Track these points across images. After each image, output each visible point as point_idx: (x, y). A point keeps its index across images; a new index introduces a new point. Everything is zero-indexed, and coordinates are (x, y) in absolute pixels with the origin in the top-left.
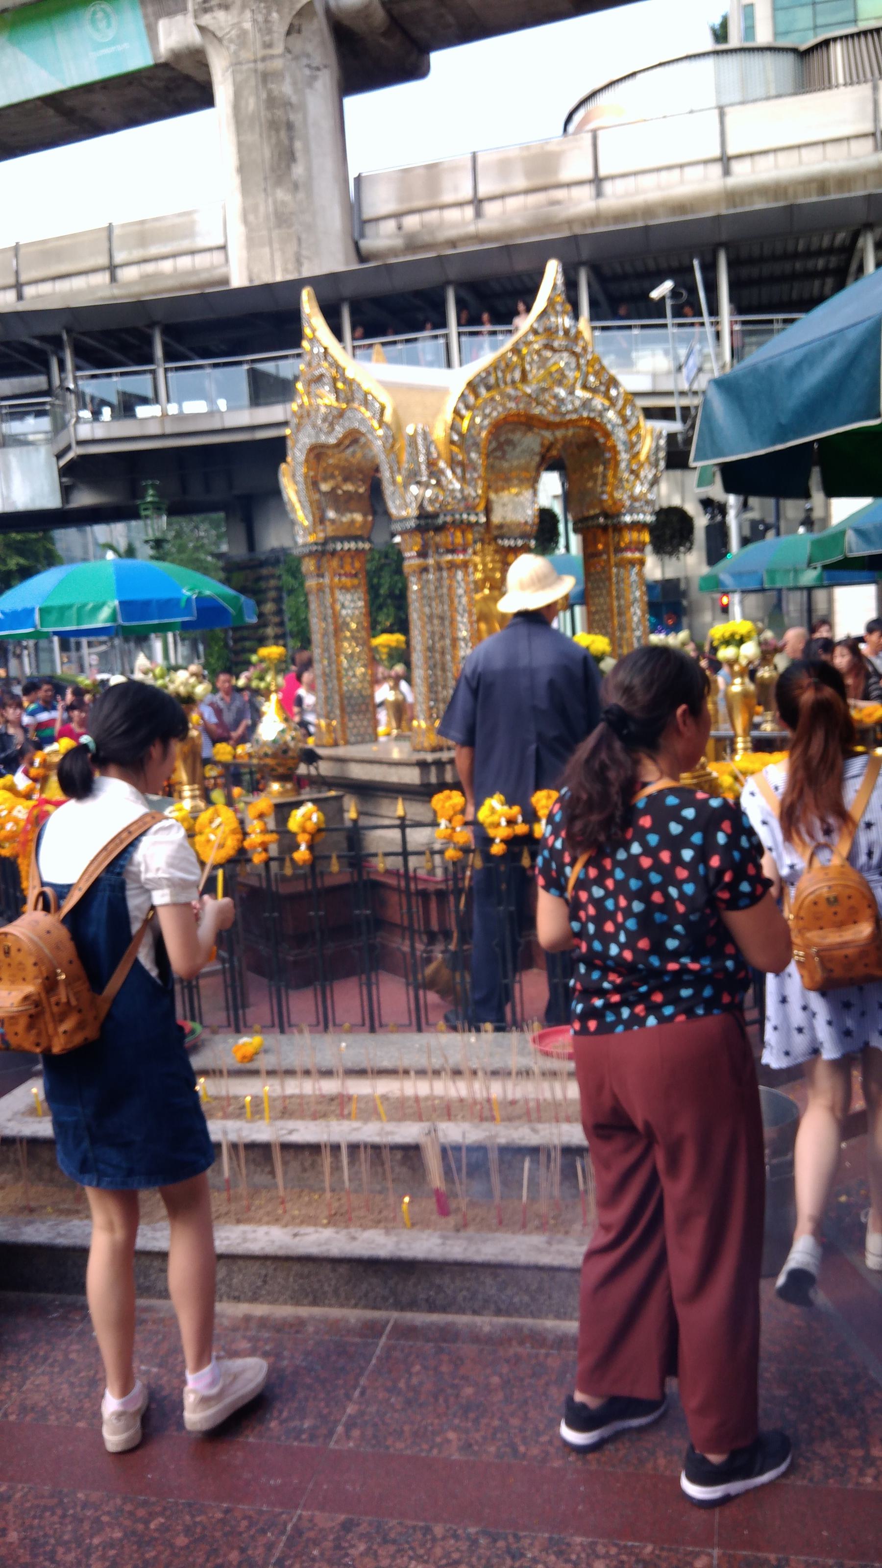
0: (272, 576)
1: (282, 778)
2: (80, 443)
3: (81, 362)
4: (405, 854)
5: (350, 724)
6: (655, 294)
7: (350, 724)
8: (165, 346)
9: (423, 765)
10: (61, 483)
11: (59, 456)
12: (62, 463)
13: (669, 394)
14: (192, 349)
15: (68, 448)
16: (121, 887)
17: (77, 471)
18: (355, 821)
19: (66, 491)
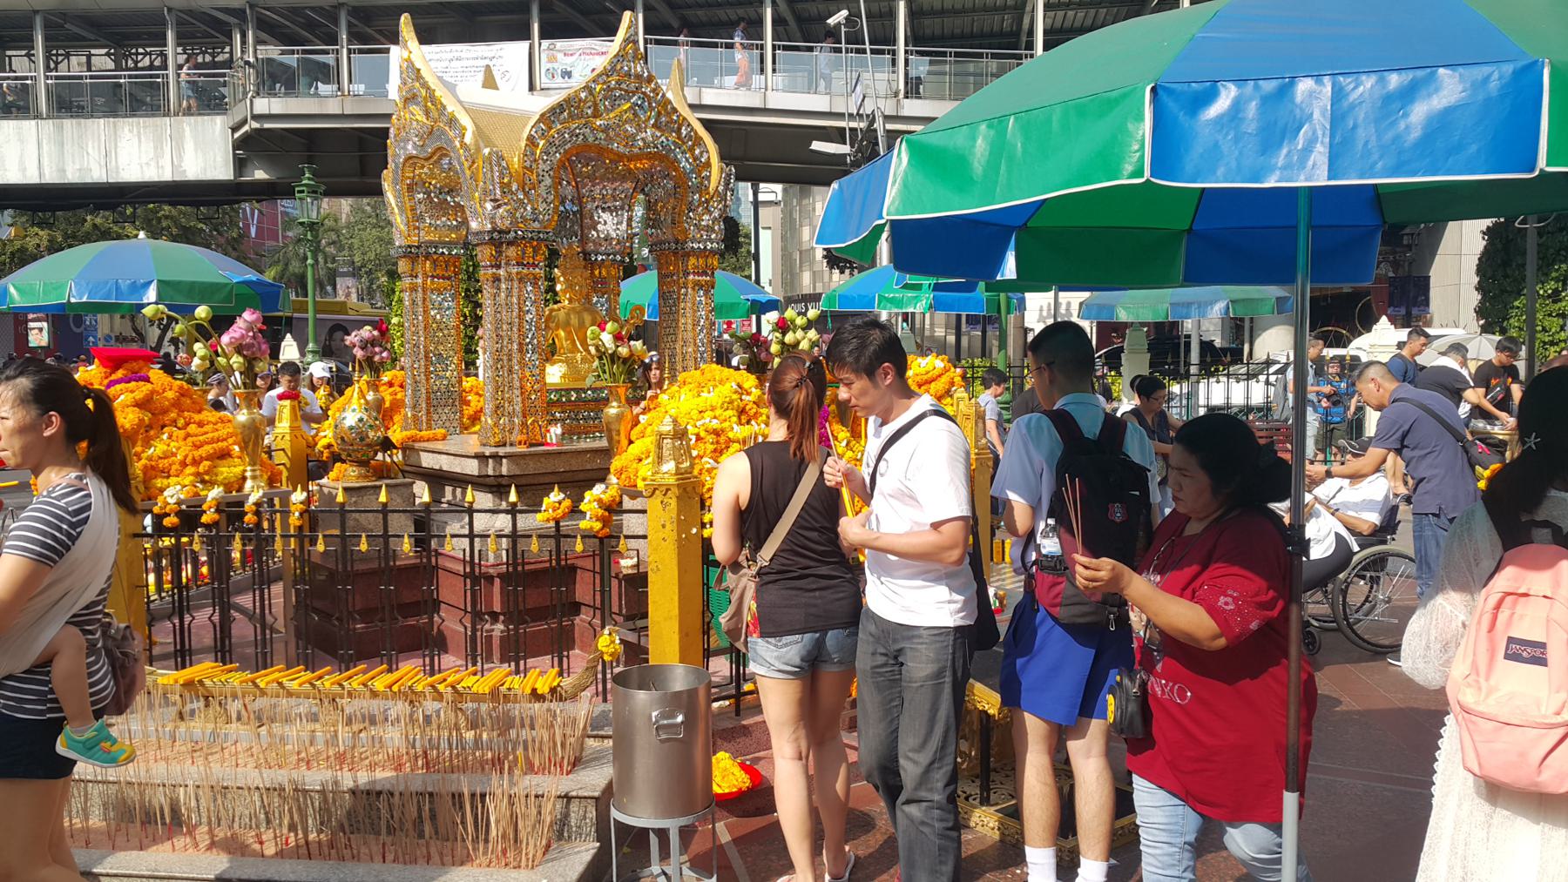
0: (1366, 143)
1: (362, 463)
2: (256, 117)
3: (264, 36)
4: (471, 536)
5: (436, 417)
6: (831, 21)
7: (436, 417)
8: (350, 25)
9: (480, 457)
10: (235, 155)
11: (234, 130)
12: (237, 135)
13: (840, 116)
14: (380, 32)
15: (244, 122)
16: (1074, 625)
17: (249, 146)
18: (427, 505)
19: (240, 164)
